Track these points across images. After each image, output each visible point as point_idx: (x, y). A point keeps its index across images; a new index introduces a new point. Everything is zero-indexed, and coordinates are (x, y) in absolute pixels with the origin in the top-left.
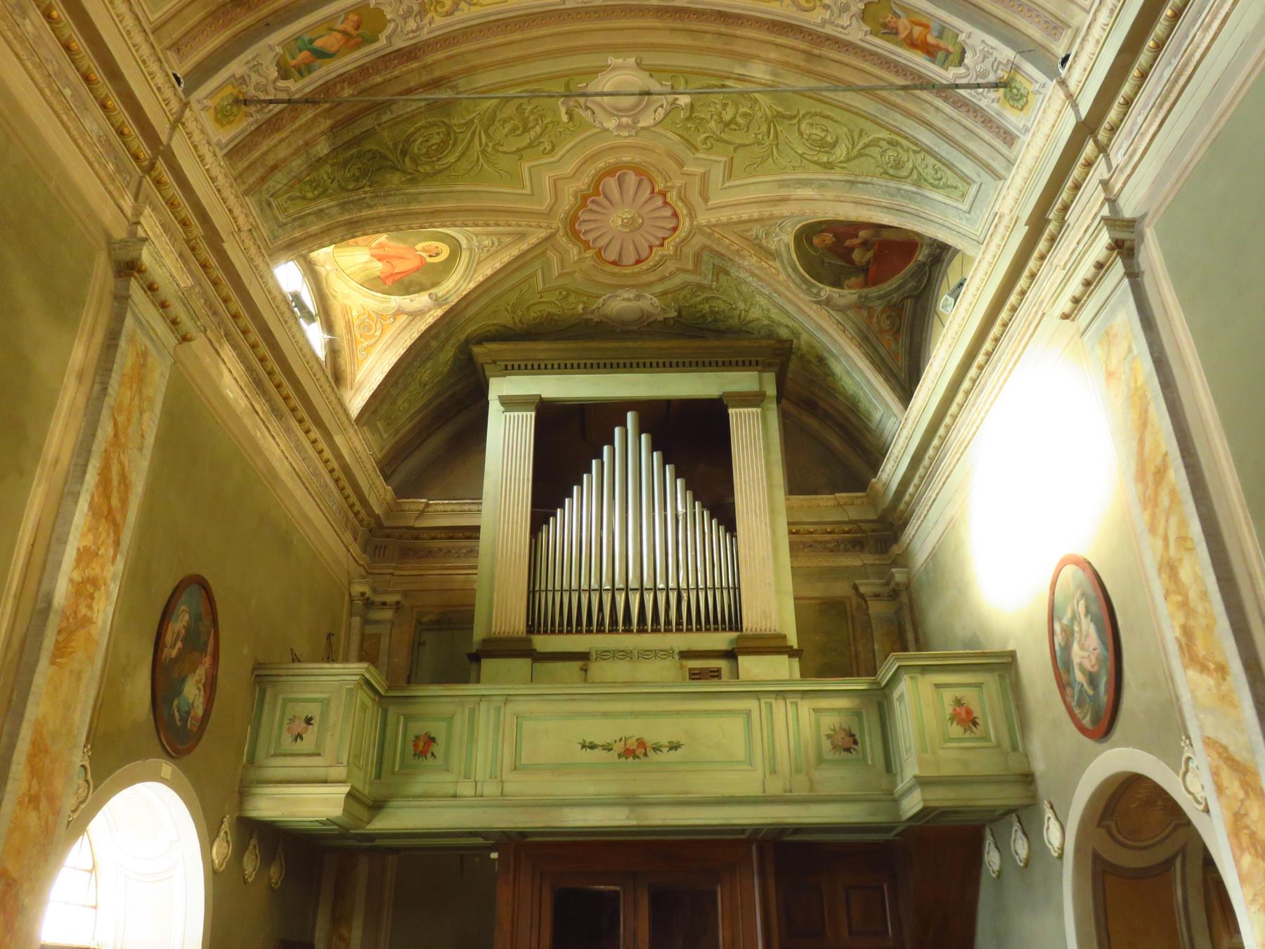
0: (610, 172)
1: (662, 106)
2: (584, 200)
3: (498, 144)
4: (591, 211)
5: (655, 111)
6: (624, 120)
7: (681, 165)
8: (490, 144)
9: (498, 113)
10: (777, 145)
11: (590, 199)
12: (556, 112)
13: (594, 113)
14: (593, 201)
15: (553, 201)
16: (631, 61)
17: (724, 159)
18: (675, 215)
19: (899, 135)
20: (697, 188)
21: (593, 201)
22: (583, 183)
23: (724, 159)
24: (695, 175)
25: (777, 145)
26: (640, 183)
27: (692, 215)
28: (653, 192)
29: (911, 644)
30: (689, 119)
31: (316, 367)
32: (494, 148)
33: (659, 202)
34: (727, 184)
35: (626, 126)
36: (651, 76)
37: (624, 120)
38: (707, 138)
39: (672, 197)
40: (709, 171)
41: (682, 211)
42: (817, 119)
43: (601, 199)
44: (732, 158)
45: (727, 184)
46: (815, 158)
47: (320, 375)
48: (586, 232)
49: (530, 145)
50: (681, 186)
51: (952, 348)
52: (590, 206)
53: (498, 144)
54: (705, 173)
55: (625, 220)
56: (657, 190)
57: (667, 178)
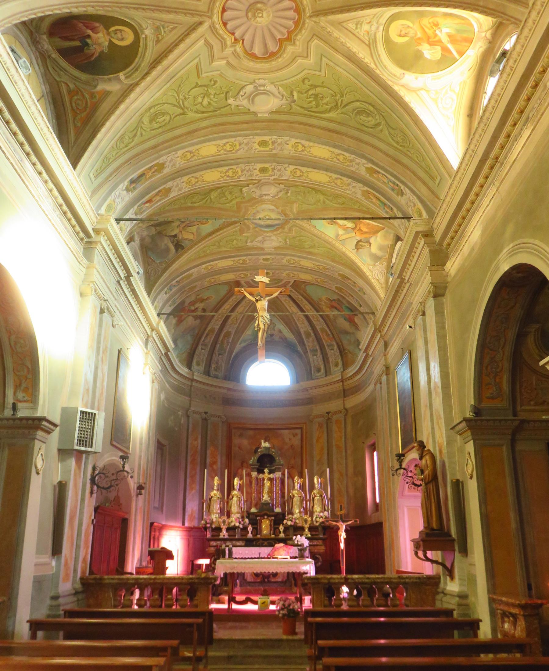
0: (272, 56)
1: (242, 96)
2: (289, 38)
3: (333, 96)
4: (285, 27)
5: (245, 93)
6: (262, 88)
7: (228, 63)
8: (337, 98)
9: (329, 110)
10: (177, 99)
11: (285, 37)
12: (299, 98)
13: (279, 93)
14: (284, 35)
15: (310, 43)
16: (259, 115)
17: (204, 75)
18: (225, 24)
19: (129, 149)
20: (215, 51)
21: (284, 35)
22: (290, 49)
23: (204, 75)
24: (218, 59)
25: (177, 99)
26: (252, 47)
27: (212, 28)
28: (243, 40)
29: (227, 556)
30: (227, 93)
31: (505, 75)
32: (336, 96)
33: (238, 34)
34: (196, 61)
35: (260, 86)
36: (249, 110)
37: (262, 88)
38: (214, 84)
39: (229, 40)
40: (210, 65)
41: (221, 31)
42: (163, 123)
43: (278, 36)
44: (198, 76)
45: (196, 61)
46: (156, 107)
47: (508, 69)
48: (290, 9)
49: (316, 87)
50: (225, 49)
51: (51, 151)
52: (285, 31)
53: (333, 96)
54: (212, 62)
55: (260, 15)
56: (241, 43)
57: (235, 53)
